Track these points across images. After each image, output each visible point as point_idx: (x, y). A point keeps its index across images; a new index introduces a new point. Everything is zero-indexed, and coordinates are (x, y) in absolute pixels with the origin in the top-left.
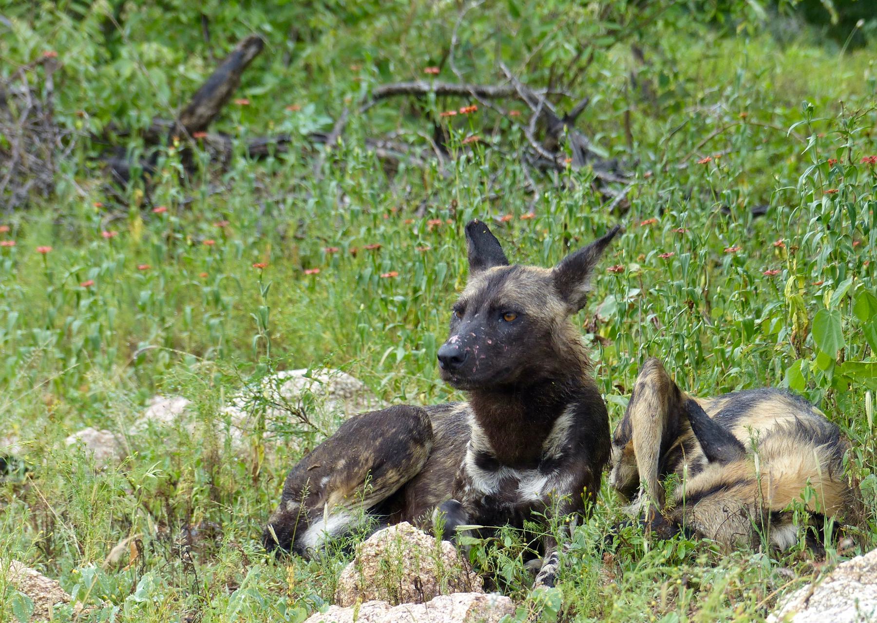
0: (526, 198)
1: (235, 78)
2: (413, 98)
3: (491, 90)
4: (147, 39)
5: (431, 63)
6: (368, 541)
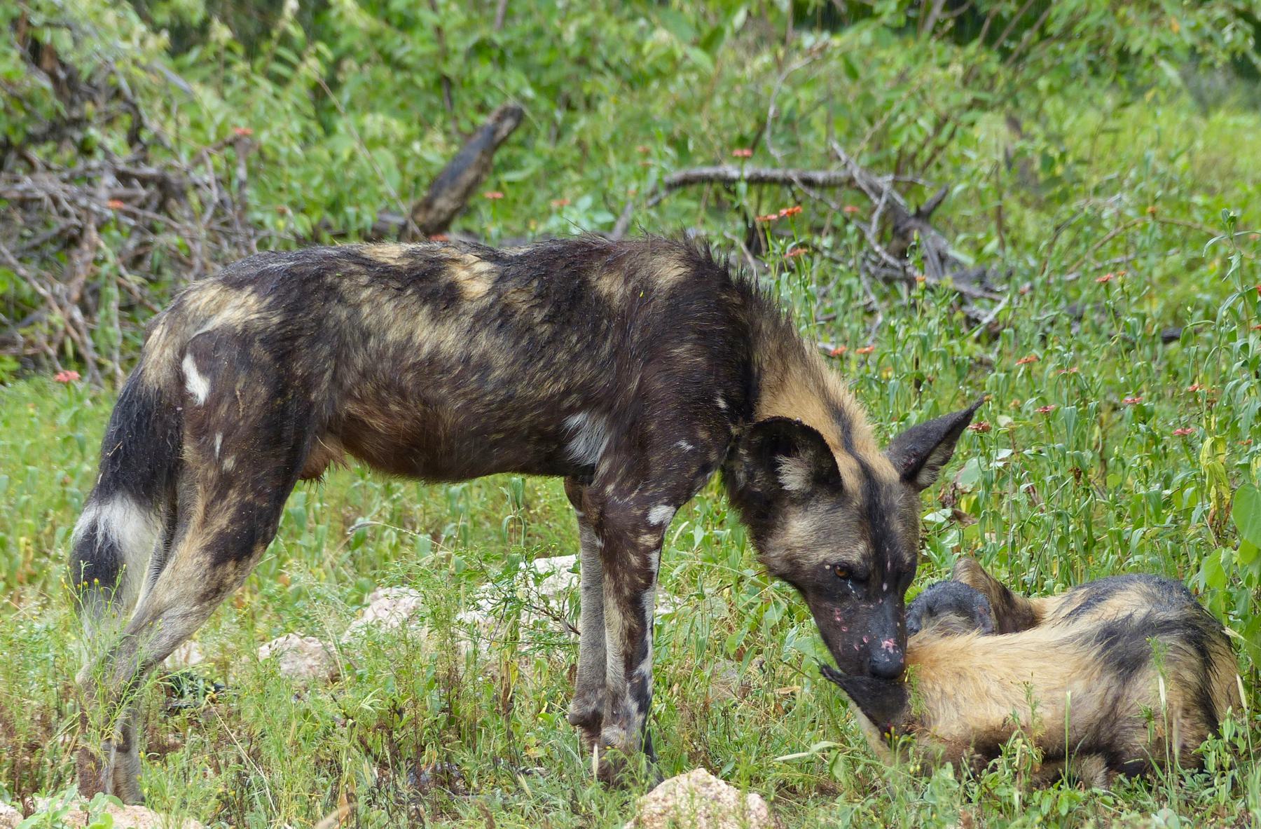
0: (866, 318)
1: (485, 160)
2: (718, 186)
3: (820, 176)
4: (372, 109)
5: (742, 141)
6: (652, 795)
